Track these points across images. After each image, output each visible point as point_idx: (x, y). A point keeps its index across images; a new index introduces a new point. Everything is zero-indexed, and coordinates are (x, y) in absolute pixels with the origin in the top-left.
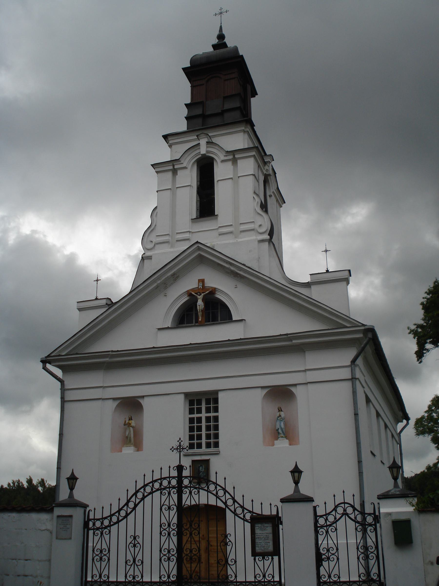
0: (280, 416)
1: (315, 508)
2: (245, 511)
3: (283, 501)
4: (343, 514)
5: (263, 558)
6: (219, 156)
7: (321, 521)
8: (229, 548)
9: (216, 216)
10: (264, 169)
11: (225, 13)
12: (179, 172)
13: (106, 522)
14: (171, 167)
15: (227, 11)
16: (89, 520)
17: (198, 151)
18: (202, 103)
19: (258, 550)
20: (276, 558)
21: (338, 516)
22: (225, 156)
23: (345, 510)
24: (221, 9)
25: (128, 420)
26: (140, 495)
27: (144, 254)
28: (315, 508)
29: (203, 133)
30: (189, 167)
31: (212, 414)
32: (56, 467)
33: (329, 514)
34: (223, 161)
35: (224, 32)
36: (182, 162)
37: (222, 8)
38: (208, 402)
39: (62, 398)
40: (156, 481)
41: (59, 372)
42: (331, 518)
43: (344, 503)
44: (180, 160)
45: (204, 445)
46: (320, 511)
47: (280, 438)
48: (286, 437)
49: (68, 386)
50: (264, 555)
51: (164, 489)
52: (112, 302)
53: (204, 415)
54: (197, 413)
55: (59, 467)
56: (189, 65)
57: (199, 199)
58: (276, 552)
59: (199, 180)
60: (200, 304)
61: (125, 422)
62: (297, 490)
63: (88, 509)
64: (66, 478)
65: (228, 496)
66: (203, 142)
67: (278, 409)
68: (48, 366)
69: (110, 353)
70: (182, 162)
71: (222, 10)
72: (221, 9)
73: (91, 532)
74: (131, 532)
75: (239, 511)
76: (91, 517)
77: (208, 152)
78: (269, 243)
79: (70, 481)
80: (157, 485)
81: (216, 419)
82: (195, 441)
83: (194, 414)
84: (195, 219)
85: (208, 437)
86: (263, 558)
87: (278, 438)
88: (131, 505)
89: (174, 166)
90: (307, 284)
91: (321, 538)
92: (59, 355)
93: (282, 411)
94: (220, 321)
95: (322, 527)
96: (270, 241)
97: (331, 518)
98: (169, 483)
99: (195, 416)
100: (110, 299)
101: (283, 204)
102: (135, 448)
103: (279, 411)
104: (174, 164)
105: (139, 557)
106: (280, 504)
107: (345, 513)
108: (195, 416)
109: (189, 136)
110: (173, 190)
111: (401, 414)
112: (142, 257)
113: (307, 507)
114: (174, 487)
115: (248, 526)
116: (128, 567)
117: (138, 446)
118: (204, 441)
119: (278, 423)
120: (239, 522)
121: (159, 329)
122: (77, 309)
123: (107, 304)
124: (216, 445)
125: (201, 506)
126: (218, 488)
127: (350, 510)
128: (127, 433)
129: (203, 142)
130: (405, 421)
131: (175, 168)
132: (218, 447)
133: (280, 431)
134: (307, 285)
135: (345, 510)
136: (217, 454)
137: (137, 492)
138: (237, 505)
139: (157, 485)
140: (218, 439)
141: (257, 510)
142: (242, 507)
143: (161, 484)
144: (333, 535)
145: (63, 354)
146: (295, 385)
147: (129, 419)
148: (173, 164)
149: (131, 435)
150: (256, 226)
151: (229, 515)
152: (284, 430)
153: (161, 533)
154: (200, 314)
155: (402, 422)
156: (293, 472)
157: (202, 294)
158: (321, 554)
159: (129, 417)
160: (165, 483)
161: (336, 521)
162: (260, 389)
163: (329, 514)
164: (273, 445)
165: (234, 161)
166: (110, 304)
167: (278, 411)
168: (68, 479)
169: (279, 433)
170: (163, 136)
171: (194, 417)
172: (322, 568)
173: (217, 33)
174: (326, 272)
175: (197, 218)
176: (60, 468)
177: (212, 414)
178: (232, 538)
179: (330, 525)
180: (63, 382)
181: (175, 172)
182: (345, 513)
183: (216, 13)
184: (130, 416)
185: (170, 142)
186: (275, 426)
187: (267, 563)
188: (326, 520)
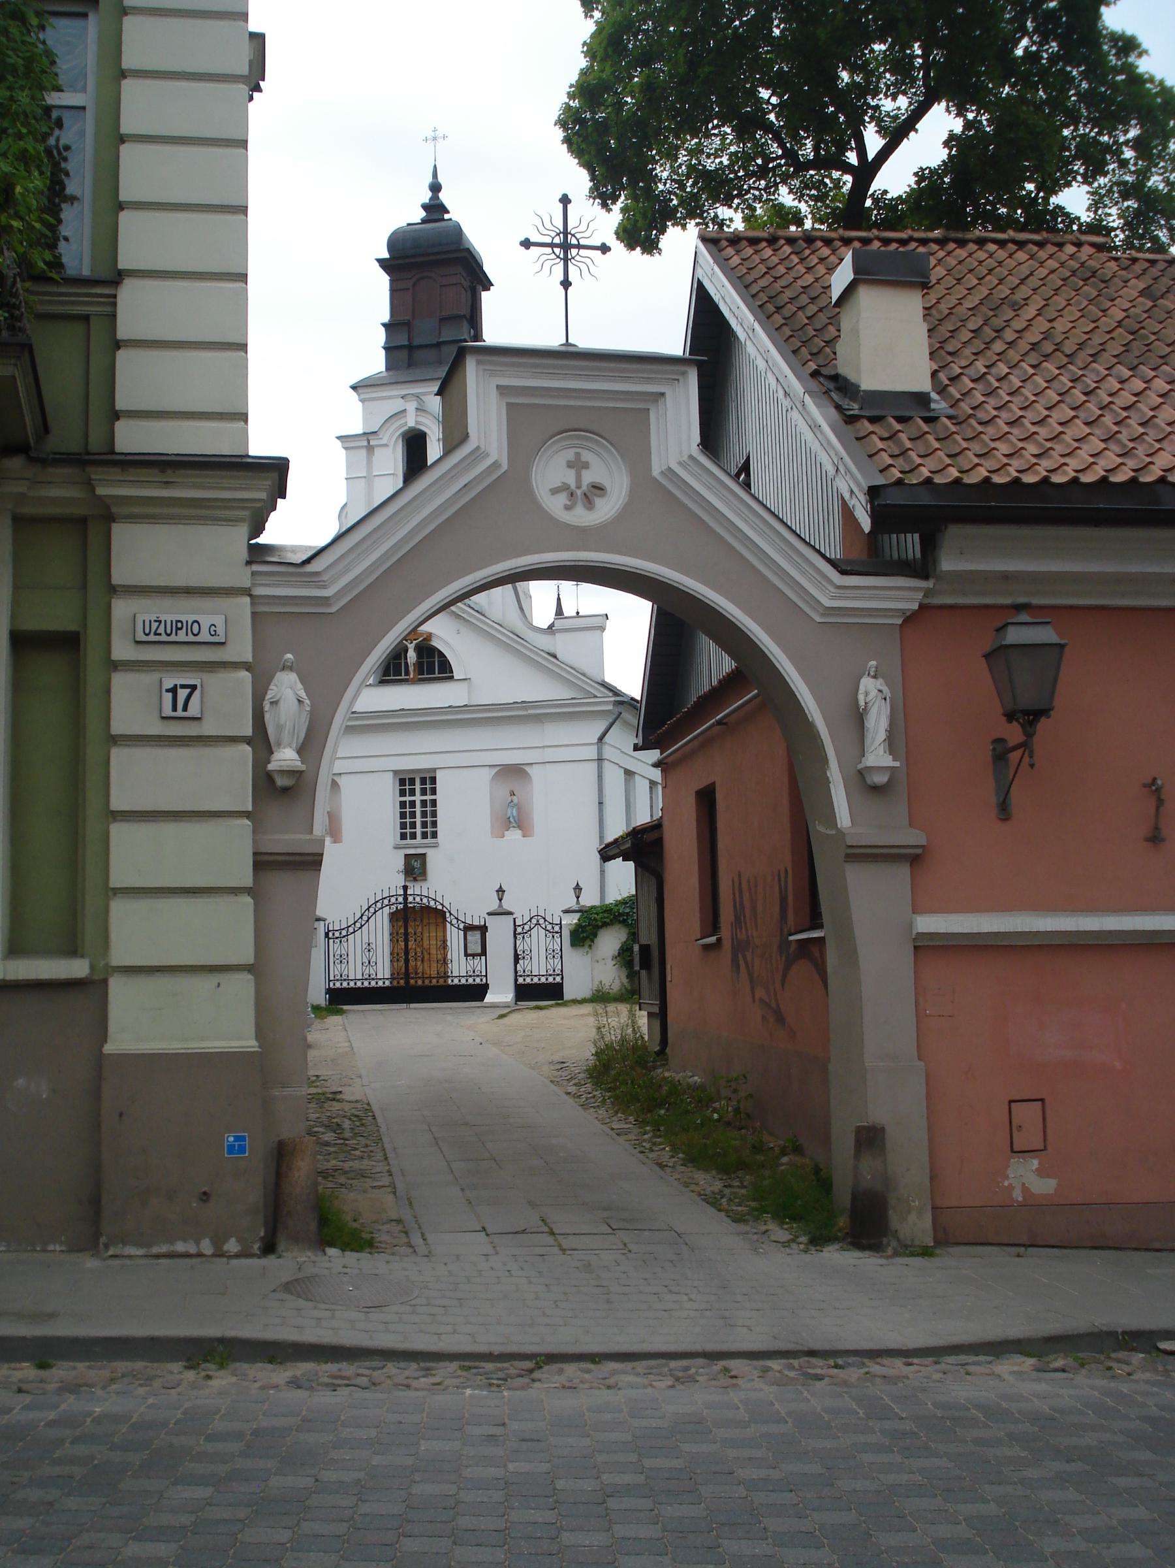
0: (512, 801)
1: (515, 919)
3: (489, 914)
7: (519, 930)
13: (344, 933)
16: (329, 931)
17: (403, 421)
18: (407, 325)
19: (469, 952)
20: (483, 958)
23: (538, 921)
26: (372, 910)
28: (515, 919)
31: (428, 797)
35: (441, 179)
38: (423, 781)
42: (527, 927)
45: (419, 835)
48: (519, 827)
50: (474, 955)
53: (418, 798)
56: (386, 255)
58: (484, 952)
60: (412, 656)
62: (500, 906)
63: (327, 923)
66: (411, 406)
73: (331, 941)
74: (365, 940)
75: (454, 922)
77: (417, 423)
80: (386, 902)
81: (434, 803)
82: (408, 830)
85: (424, 825)
88: (365, 918)
89: (369, 441)
91: (518, 942)
94: (439, 674)
95: (520, 934)
97: (527, 927)
98: (397, 899)
99: (408, 799)
105: (373, 959)
106: (487, 916)
107: (538, 924)
108: (408, 799)
113: (511, 918)
115: (462, 933)
116: (364, 968)
118: (419, 830)
119: (509, 811)
120: (455, 930)
127: (542, 921)
131: (371, 444)
132: (436, 838)
133: (511, 819)
135: (538, 921)
136: (436, 846)
138: (452, 917)
139: (386, 902)
140: (436, 807)
142: (457, 919)
143: (389, 901)
144: (528, 940)
152: (516, 819)
153: (562, 971)
154: (411, 669)
157: (414, 642)
158: (518, 955)
162: (488, 768)
169: (510, 822)
173: (430, 179)
181: (370, 449)
182: (538, 924)
186: (506, 814)
187: (476, 962)
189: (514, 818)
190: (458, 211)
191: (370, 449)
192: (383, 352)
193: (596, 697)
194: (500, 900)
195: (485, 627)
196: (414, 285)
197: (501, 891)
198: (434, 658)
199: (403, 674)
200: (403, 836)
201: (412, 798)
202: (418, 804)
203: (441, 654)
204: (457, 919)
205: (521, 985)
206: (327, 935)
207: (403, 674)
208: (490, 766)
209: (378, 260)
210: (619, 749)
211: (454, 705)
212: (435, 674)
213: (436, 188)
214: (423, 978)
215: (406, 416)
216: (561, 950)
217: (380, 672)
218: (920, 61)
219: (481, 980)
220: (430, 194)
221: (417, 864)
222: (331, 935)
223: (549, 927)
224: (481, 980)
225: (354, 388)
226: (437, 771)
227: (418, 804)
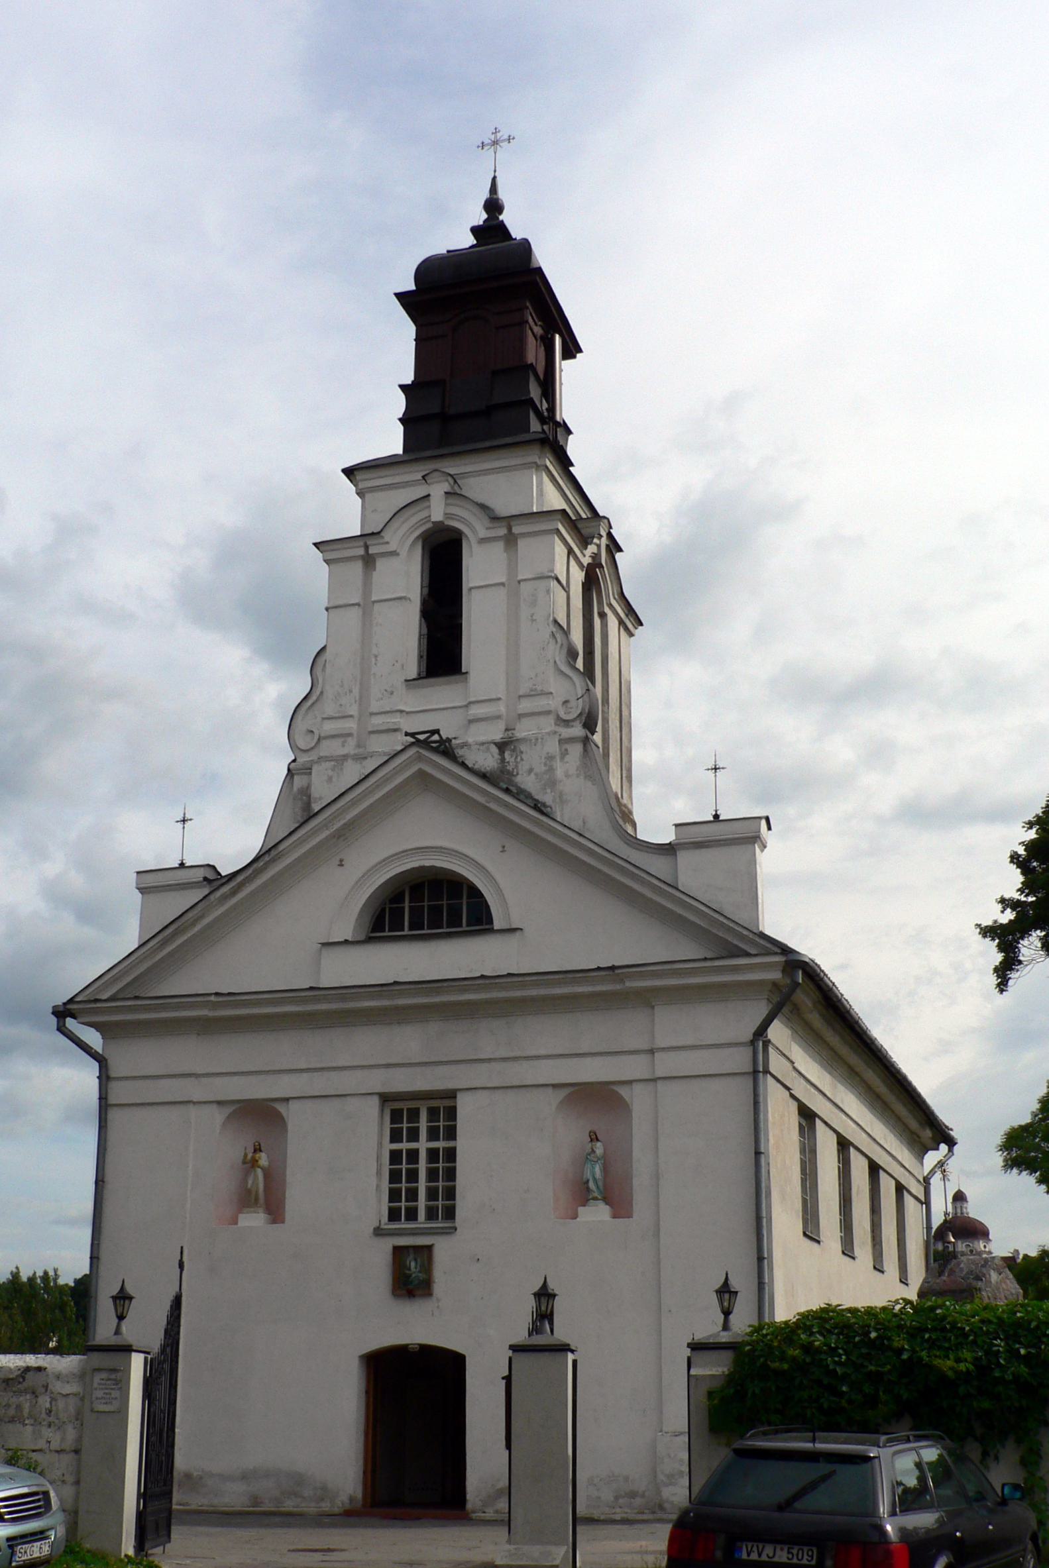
0: (593, 1151)
6: (474, 529)
9: (464, 676)
10: (584, 556)
11: (506, 143)
12: (380, 564)
15: (509, 139)
22: (487, 529)
24: (496, 132)
25: (253, 1151)
27: (294, 761)
29: (436, 470)
30: (404, 553)
32: (88, 1255)
34: (483, 541)
35: (502, 195)
37: (497, 130)
38: (433, 1113)
39: (103, 1098)
41: (93, 1038)
44: (382, 534)
47: (591, 1201)
48: (606, 1200)
49: (118, 1068)
52: (219, 874)
53: (404, 1185)
54: (408, 1141)
55: (95, 1255)
56: (411, 286)
57: (425, 631)
59: (426, 582)
61: (246, 1155)
64: (112, 1295)
66: (438, 490)
67: (590, 1136)
68: (70, 1023)
69: (213, 998)
70: (387, 539)
71: (499, 135)
72: (496, 131)
77: (448, 516)
79: (118, 1302)
81: (451, 1154)
83: (402, 1142)
84: (414, 679)
87: (588, 1200)
89: (367, 547)
90: (667, 847)
92: (97, 1001)
93: (598, 1140)
99: (404, 1146)
100: (213, 867)
101: (636, 628)
102: (266, 1215)
103: (592, 1140)
104: (368, 543)
108: (404, 1146)
109: (406, 473)
110: (366, 606)
111: (928, 1133)
117: (275, 1212)
121: (324, 944)
122: (138, 889)
123: (205, 879)
124: (450, 1213)
125: (413, 1348)
128: (250, 1182)
129: (438, 490)
130: (944, 1148)
131: (370, 552)
133: (591, 1185)
134: (668, 849)
145: (105, 997)
146: (630, 1082)
147: (255, 1151)
148: (365, 544)
149: (257, 1184)
150: (554, 703)
155: (937, 1149)
159: (254, 1146)
162: (550, 1090)
164: (575, 1217)
165: (511, 541)
166: (212, 879)
167: (590, 1140)
168: (115, 1298)
169: (588, 1190)
170: (345, 471)
171: (400, 1148)
173: (485, 195)
174: (712, 819)
175: (420, 678)
176: (98, 1258)
177: (440, 1144)
180: (104, 1062)
181: (369, 561)
183: (483, 143)
184: (257, 1144)
185: (361, 486)
189: (595, 1180)
190: (516, 222)
193: (748, 955)
195: (550, 838)
198: (461, 898)
200: (394, 1215)
201: (413, 1145)
202: (423, 1156)
203: (475, 892)
209: (400, 296)
210: (788, 1089)
212: (461, 926)
215: (429, 507)
218: (814, 1330)
220: (485, 216)
226: (459, 1096)
227: (423, 1156)
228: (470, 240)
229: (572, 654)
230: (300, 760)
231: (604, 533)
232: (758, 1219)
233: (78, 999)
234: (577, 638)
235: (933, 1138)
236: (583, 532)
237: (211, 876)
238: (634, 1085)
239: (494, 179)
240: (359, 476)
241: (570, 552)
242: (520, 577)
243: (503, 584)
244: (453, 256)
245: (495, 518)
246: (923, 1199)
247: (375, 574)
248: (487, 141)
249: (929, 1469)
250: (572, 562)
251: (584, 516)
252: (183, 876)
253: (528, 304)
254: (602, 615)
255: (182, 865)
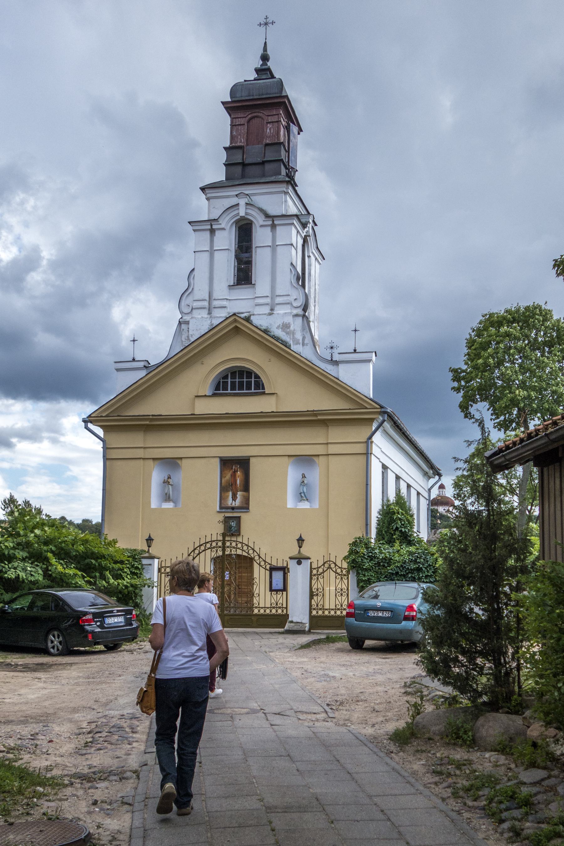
0: (303, 482)
2: (267, 564)
4: (328, 568)
5: (277, 593)
6: (258, 220)
7: (315, 572)
8: (255, 587)
12: (217, 233)
14: (209, 227)
19: (273, 588)
20: (285, 593)
21: (325, 569)
28: (311, 563)
30: (228, 228)
33: (320, 567)
35: (269, 52)
36: (220, 222)
40: (208, 542)
41: (100, 432)
42: (321, 570)
43: (330, 561)
46: (314, 566)
50: (277, 591)
51: (213, 548)
58: (285, 589)
65: (255, 554)
66: (242, 202)
68: (90, 426)
69: (151, 417)
70: (220, 222)
72: (267, 18)
75: (262, 563)
76: (163, 565)
77: (246, 214)
78: (303, 318)
86: (277, 593)
89: (211, 225)
91: (313, 582)
95: (315, 575)
96: (304, 316)
97: (321, 570)
100: (147, 361)
106: (288, 560)
110: (212, 252)
111: (431, 472)
112: (179, 322)
114: (220, 547)
115: (268, 572)
121: (196, 396)
123: (145, 366)
126: (249, 548)
129: (242, 202)
135: (330, 565)
137: (195, 549)
138: (261, 560)
139: (208, 545)
141: (274, 563)
142: (265, 561)
143: (211, 545)
144: (321, 580)
150: (291, 299)
151: (256, 566)
156: (298, 540)
158: (313, 592)
160: (214, 544)
161: (324, 572)
162: (287, 457)
163: (320, 567)
165: (273, 227)
169: (301, 496)
172: (313, 600)
173: (261, 52)
178: (257, 580)
179: (320, 574)
181: (212, 231)
182: (330, 567)
185: (209, 195)
187: (279, 596)
188: (318, 571)
191: (212, 231)
192: (224, 168)
193: (366, 408)
194: (300, 547)
196: (248, 122)
197: (300, 541)
199: (229, 389)
203: (257, 377)
204: (265, 561)
205: (314, 616)
206: (159, 570)
207: (229, 389)
208: (289, 456)
209: (223, 103)
211: (264, 411)
213: (265, 58)
214: (323, 609)
216: (348, 589)
217: (214, 387)
219: (283, 611)
221: (233, 524)
222: (163, 570)
223: (339, 571)
224: (283, 611)
225: (203, 189)
228: (254, 75)
229: (298, 279)
230: (184, 318)
231: (311, 221)
232: (367, 485)
233: (92, 416)
234: (299, 269)
235: (433, 473)
236: (302, 220)
237: (147, 365)
238: (320, 457)
239: (265, 43)
240: (207, 191)
241: (298, 232)
242: (277, 244)
243: (270, 246)
244: (248, 84)
245: (267, 216)
246: (427, 498)
247: (215, 237)
248: (262, 23)
249: (174, 743)
250: (299, 236)
251: (303, 213)
252: (135, 365)
253: (281, 112)
254: (309, 257)
255: (134, 360)
